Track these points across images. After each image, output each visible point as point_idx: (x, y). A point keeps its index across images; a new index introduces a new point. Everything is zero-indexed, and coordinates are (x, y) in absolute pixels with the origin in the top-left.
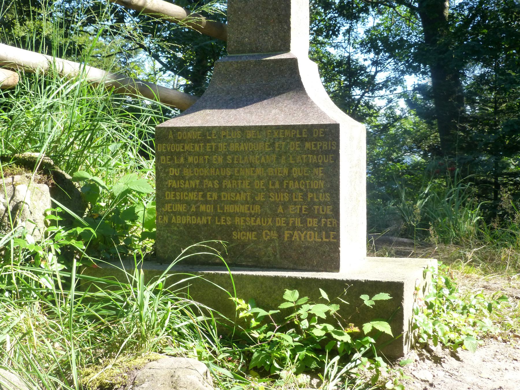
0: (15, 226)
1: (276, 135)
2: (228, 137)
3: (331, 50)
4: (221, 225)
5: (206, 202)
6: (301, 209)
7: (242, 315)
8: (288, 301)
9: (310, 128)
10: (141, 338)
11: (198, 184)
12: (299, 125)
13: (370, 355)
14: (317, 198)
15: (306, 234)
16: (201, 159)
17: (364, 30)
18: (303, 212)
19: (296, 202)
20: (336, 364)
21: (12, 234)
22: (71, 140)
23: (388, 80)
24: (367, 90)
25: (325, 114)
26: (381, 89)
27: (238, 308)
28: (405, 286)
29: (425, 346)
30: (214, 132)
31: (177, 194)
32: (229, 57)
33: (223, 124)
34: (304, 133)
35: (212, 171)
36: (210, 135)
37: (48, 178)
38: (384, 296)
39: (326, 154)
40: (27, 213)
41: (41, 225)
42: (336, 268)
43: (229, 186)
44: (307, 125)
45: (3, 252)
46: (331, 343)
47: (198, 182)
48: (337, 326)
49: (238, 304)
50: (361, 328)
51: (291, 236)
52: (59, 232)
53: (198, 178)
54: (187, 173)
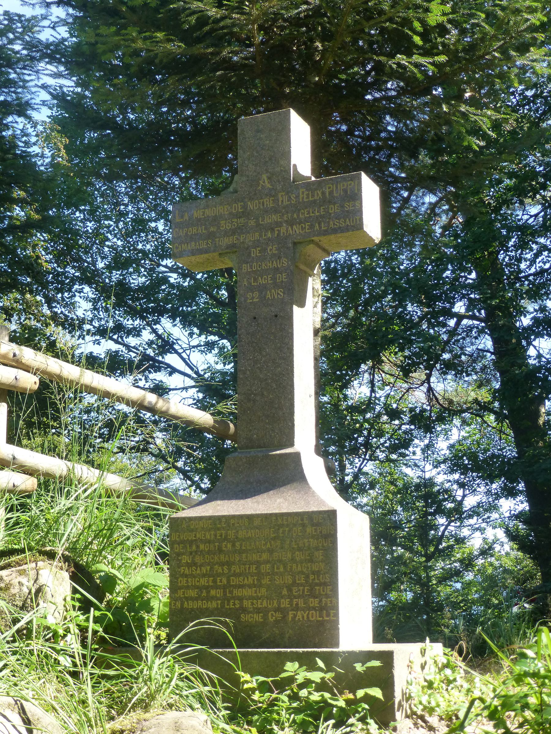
0: (37, 606)
1: (280, 522)
2: (236, 525)
3: (408, 471)
4: (230, 609)
5: (216, 587)
6: (303, 590)
7: (246, 686)
8: (288, 671)
9: (310, 515)
10: (151, 697)
11: (208, 569)
12: (300, 512)
13: (363, 720)
14: (318, 579)
15: (309, 613)
16: (212, 546)
17: (448, 444)
18: (306, 593)
19: (298, 584)
20: (331, 726)
21: (34, 613)
22: (90, 540)
23: (479, 505)
24: (453, 519)
25: (324, 502)
26: (470, 517)
27: (242, 680)
28: (395, 654)
29: (422, 718)
30: (224, 520)
31: (189, 580)
32: (239, 453)
33: (232, 512)
34: (305, 519)
35: (222, 557)
36: (220, 522)
37: (68, 566)
38: (376, 663)
39: (325, 538)
40: (49, 596)
41: (61, 608)
42: (337, 645)
43: (238, 571)
44: (308, 512)
45: (25, 632)
46: (328, 709)
47: (208, 568)
48: (334, 694)
49: (243, 677)
50: (354, 695)
51: (295, 616)
52: (78, 616)
53: (209, 564)
54: (198, 559)
